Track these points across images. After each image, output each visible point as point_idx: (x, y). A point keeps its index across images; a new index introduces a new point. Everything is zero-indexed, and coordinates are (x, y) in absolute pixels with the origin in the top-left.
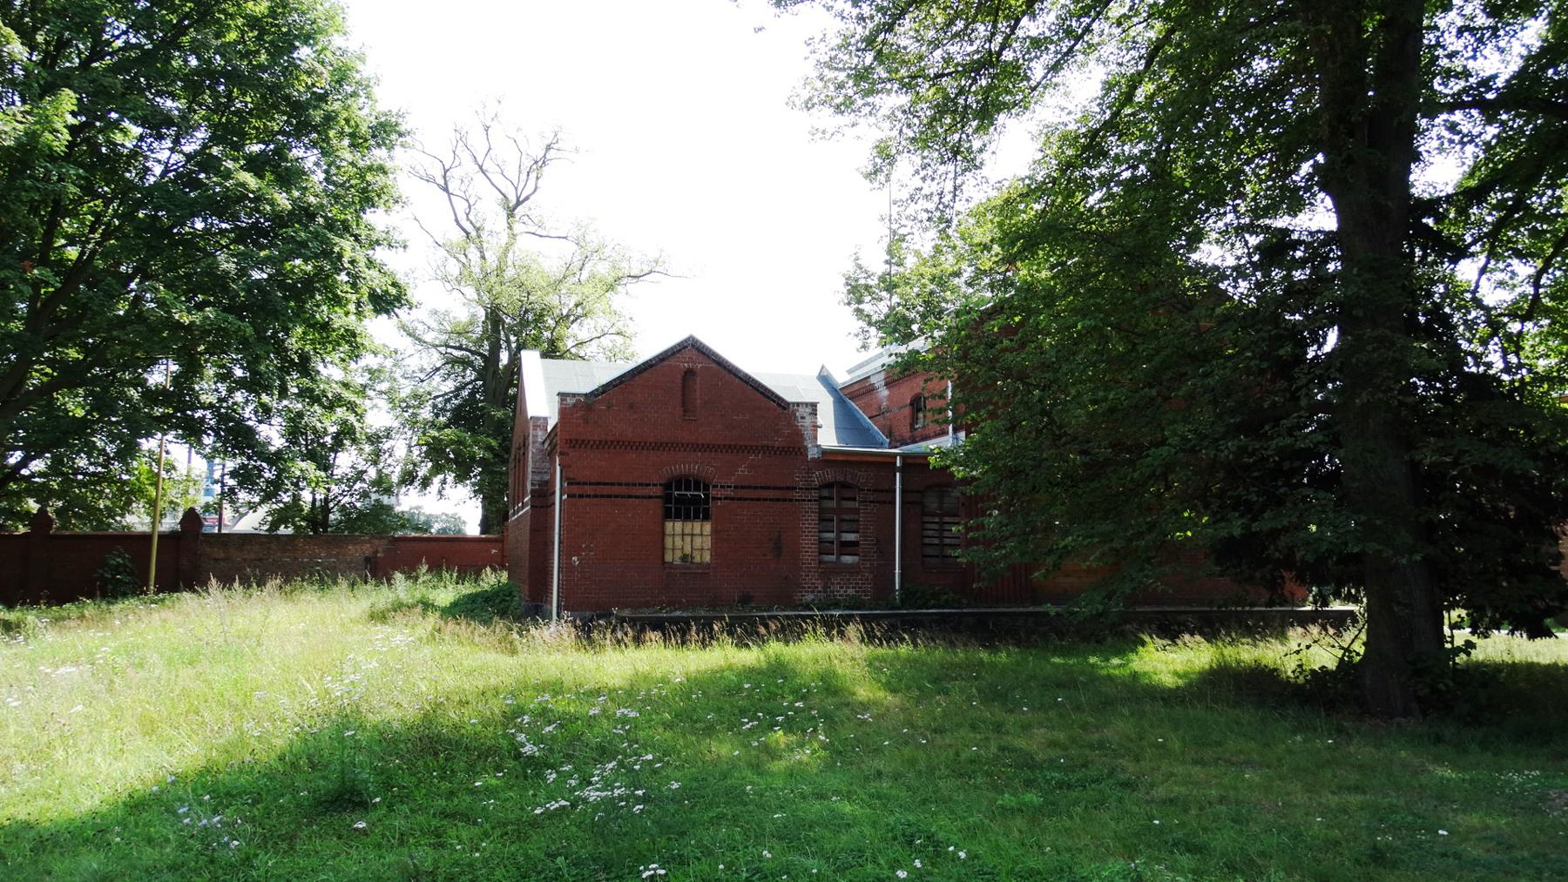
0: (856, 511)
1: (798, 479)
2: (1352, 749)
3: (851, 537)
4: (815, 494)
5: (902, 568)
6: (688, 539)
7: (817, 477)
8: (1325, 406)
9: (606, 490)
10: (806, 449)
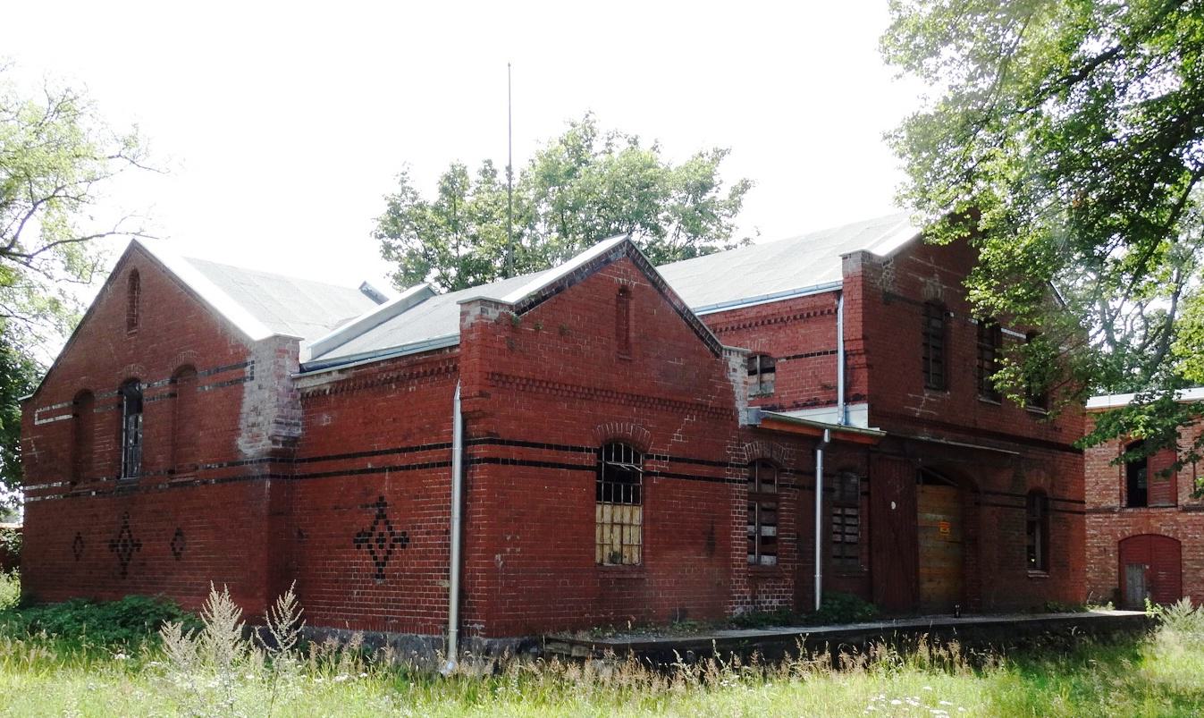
1: (730, 453)
2: (1143, 669)
3: (769, 531)
4: (745, 473)
5: (823, 571)
6: (617, 529)
7: (752, 449)
8: (1141, 155)
9: (535, 454)
10: (737, 412)
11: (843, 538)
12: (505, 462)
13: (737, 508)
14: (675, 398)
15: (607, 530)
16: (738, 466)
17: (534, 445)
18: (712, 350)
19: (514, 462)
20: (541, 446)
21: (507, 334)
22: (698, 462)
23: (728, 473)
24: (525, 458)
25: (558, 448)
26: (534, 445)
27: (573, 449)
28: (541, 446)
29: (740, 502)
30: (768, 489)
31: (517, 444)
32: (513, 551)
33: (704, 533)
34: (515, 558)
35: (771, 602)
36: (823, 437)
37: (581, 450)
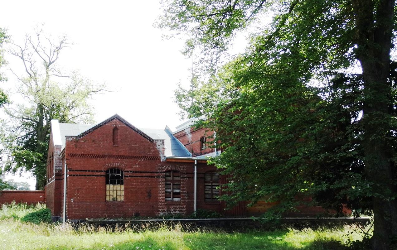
0: (179, 181)
1: (157, 169)
3: (178, 191)
4: (164, 175)
6: (115, 192)
7: (164, 168)
11: (212, 192)
12: (74, 176)
13: (161, 184)
14: (135, 155)
15: (111, 192)
16: (160, 173)
17: (84, 171)
18: (150, 140)
19: (77, 175)
20: (86, 171)
21: (75, 144)
22: (143, 172)
23: (156, 175)
24: (81, 174)
25: (92, 171)
26: (84, 171)
27: (97, 171)
28: (86, 171)
29: (162, 183)
30: (176, 178)
31: (78, 171)
32: (76, 198)
33: (147, 192)
34: (77, 200)
35: (175, 212)
36: (194, 163)
37: (100, 171)
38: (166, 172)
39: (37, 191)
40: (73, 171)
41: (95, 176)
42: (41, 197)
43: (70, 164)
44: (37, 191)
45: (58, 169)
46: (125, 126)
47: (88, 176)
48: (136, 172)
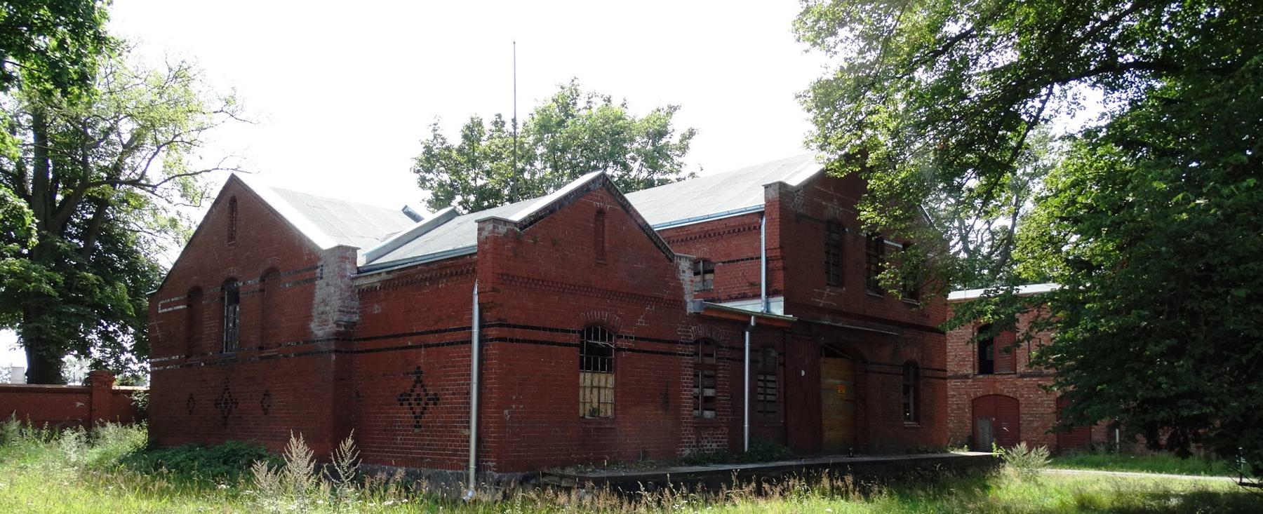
0: (714, 367)
3: (709, 392)
4: (691, 349)
6: (595, 391)
9: (534, 335)
19: (518, 341)
23: (679, 349)
27: (563, 331)
30: (708, 360)
31: (521, 327)
36: (766, 321)
37: (569, 331)
38: (697, 342)
39: (33, 386)
40: (509, 326)
41: (560, 344)
42: (79, 404)
43: (501, 305)
44: (33, 386)
45: (345, 319)
46: (619, 208)
47: (542, 343)
48: (642, 339)
